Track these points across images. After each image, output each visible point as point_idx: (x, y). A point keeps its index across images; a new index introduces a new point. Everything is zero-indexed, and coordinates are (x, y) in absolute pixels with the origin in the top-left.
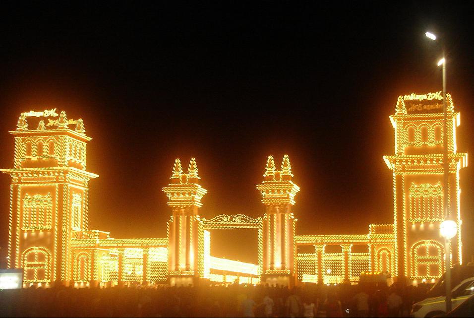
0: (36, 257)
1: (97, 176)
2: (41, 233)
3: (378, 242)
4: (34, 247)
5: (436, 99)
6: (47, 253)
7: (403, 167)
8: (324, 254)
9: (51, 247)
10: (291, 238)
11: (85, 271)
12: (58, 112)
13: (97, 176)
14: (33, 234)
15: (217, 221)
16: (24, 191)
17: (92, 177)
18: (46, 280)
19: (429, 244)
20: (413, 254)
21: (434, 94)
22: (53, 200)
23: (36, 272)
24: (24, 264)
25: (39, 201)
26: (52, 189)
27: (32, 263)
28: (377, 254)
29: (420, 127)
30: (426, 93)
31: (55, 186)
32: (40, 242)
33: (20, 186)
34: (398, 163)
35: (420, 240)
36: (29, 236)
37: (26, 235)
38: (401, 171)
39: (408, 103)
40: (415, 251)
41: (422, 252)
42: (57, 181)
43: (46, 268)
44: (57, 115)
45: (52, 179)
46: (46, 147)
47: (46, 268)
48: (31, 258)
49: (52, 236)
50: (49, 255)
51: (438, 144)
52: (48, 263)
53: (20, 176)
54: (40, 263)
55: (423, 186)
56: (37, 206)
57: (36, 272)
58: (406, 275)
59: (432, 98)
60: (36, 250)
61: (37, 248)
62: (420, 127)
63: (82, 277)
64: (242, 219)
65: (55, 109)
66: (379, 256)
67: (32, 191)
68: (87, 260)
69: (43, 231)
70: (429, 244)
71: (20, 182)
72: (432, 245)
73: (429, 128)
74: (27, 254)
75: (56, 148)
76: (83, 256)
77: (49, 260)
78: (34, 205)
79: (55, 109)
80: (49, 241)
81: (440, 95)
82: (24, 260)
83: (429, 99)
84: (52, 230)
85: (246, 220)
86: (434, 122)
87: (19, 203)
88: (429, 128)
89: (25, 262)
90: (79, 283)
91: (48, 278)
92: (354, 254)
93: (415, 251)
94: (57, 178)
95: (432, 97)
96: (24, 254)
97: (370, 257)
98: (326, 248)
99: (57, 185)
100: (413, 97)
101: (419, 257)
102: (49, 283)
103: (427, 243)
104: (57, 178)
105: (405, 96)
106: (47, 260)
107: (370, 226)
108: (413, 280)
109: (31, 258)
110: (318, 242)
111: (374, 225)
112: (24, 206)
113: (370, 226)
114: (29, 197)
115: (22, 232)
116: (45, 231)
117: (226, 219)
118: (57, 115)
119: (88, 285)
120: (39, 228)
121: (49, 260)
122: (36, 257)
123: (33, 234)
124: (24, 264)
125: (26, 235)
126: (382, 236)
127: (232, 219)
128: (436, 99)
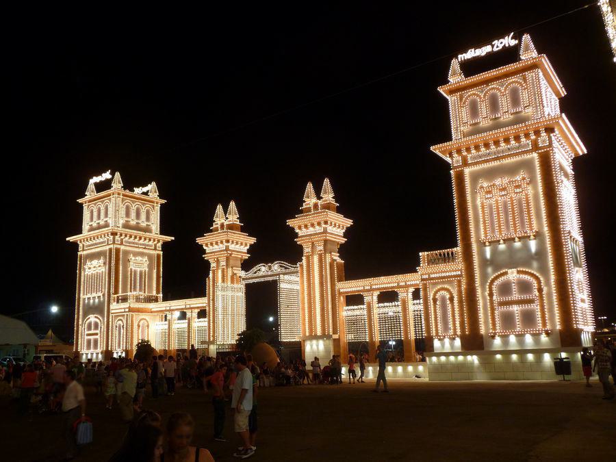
0: (514, 288)
3: (433, 279)
4: (510, 271)
5: (507, 45)
8: (375, 305)
10: (333, 285)
11: (121, 343)
12: (518, 37)
15: (255, 273)
16: (475, 177)
18: (99, 349)
20: (491, 295)
21: (501, 40)
22: (532, 181)
24: (491, 300)
25: (504, 189)
26: (528, 165)
28: (432, 297)
30: (488, 41)
31: (533, 159)
39: (470, 68)
41: (505, 289)
44: (517, 42)
45: (151, 246)
46: (483, 105)
47: (536, 307)
51: (147, 225)
53: (465, 153)
55: (498, 182)
58: (483, 331)
59: (501, 47)
60: (513, 275)
63: (119, 347)
64: (281, 266)
66: (435, 300)
67: (490, 174)
68: (452, 299)
71: (465, 163)
72: (521, 276)
74: (496, 283)
75: (524, 96)
76: (443, 292)
77: (540, 290)
78: (497, 198)
82: (491, 295)
83: (495, 49)
85: (286, 268)
87: (469, 198)
89: (495, 298)
90: (117, 353)
92: (382, 305)
95: (499, 45)
97: (365, 312)
98: (199, 313)
99: (535, 155)
100: (471, 54)
103: (512, 273)
105: (460, 56)
107: (421, 254)
108: (493, 337)
110: (367, 288)
111: (426, 253)
112: (479, 202)
113: (421, 254)
114: (485, 185)
117: (263, 269)
118: (517, 42)
119: (124, 355)
120: (498, 236)
121: (540, 290)
122: (514, 288)
124: (491, 300)
125: (488, 251)
126: (442, 267)
127: (270, 267)
128: (507, 45)
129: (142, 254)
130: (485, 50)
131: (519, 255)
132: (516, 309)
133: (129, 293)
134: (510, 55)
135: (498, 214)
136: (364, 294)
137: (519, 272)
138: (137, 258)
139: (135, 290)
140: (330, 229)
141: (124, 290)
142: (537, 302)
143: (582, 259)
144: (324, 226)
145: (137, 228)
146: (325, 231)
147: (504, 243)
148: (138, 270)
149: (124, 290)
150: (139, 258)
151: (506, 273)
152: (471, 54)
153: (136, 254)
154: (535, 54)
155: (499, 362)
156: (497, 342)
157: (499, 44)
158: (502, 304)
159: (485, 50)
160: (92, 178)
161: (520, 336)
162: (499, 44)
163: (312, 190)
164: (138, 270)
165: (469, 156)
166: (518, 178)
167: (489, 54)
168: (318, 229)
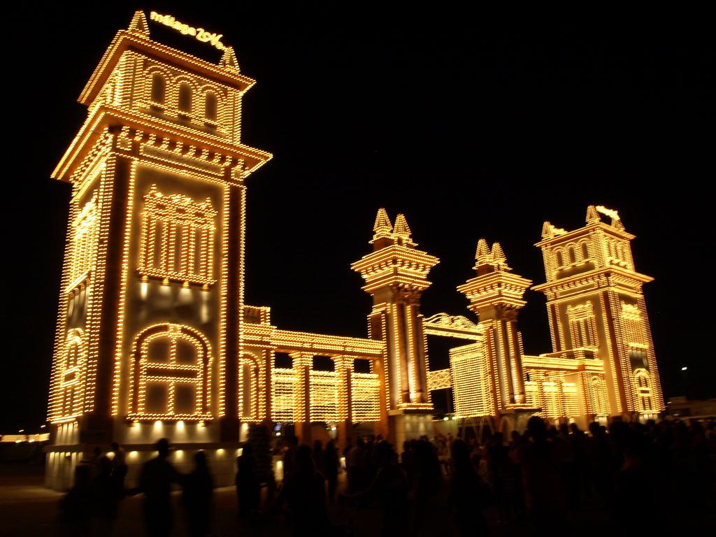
0: (173, 350)
1: (651, 279)
2: (185, 291)
4: (171, 326)
6: (202, 342)
7: (136, 146)
9: (210, 329)
13: (651, 279)
14: (165, 289)
17: (647, 281)
18: (198, 412)
19: (179, 334)
21: (208, 34)
22: (218, 219)
23: (172, 390)
24: (137, 366)
27: (162, 366)
29: (179, 80)
32: (186, 312)
33: (135, 163)
34: (123, 135)
35: (164, 322)
36: (153, 293)
37: (144, 289)
38: (127, 153)
39: (159, 32)
40: (144, 348)
42: (227, 177)
43: (198, 381)
47: (198, 381)
48: (159, 351)
49: (213, 304)
50: (205, 350)
52: (205, 369)
54: (186, 367)
55: (176, 198)
56: (178, 222)
57: (172, 390)
59: (205, 40)
60: (174, 332)
61: (179, 326)
62: (179, 80)
65: (221, 36)
69: (192, 285)
70: (179, 334)
73: (170, 80)
74: (199, 347)
77: (206, 361)
79: (221, 36)
80: (204, 313)
81: (221, 40)
82: (138, 356)
84: (213, 288)
86: (180, 73)
88: (170, 80)
89: (143, 361)
91: (205, 410)
93: (144, 348)
94: (228, 170)
96: (140, 342)
100: (168, 21)
101: (153, 365)
102: (207, 423)
103: (175, 330)
104: (228, 170)
106: (200, 361)
109: (159, 351)
112: (144, 214)
115: (136, 276)
116: (195, 286)
120: (161, 272)
121: (206, 361)
122: (173, 350)
123: (165, 289)
124: (137, 366)
125: (144, 289)
129: (583, 301)
130: (185, 30)
131: (164, 304)
132: (172, 381)
133: (574, 350)
134: (212, 54)
135: (148, 233)
136: (293, 354)
137: (184, 331)
138: (576, 308)
139: (582, 345)
140: (505, 291)
141: (569, 346)
142: (199, 378)
143: (66, 310)
144: (393, 266)
145: (576, 271)
146: (500, 295)
147: (189, 288)
148: (581, 320)
149: (569, 346)
150: (580, 307)
151: (165, 328)
152: (168, 21)
153: (574, 303)
154: (236, 69)
155: (221, 459)
156: (136, 428)
157: (203, 36)
158: (151, 372)
159: (185, 30)
160: (601, 205)
161: (170, 424)
162: (203, 36)
163: (386, 216)
164: (581, 320)
165: (143, 145)
166: (203, 205)
167: (188, 36)
168: (389, 270)
